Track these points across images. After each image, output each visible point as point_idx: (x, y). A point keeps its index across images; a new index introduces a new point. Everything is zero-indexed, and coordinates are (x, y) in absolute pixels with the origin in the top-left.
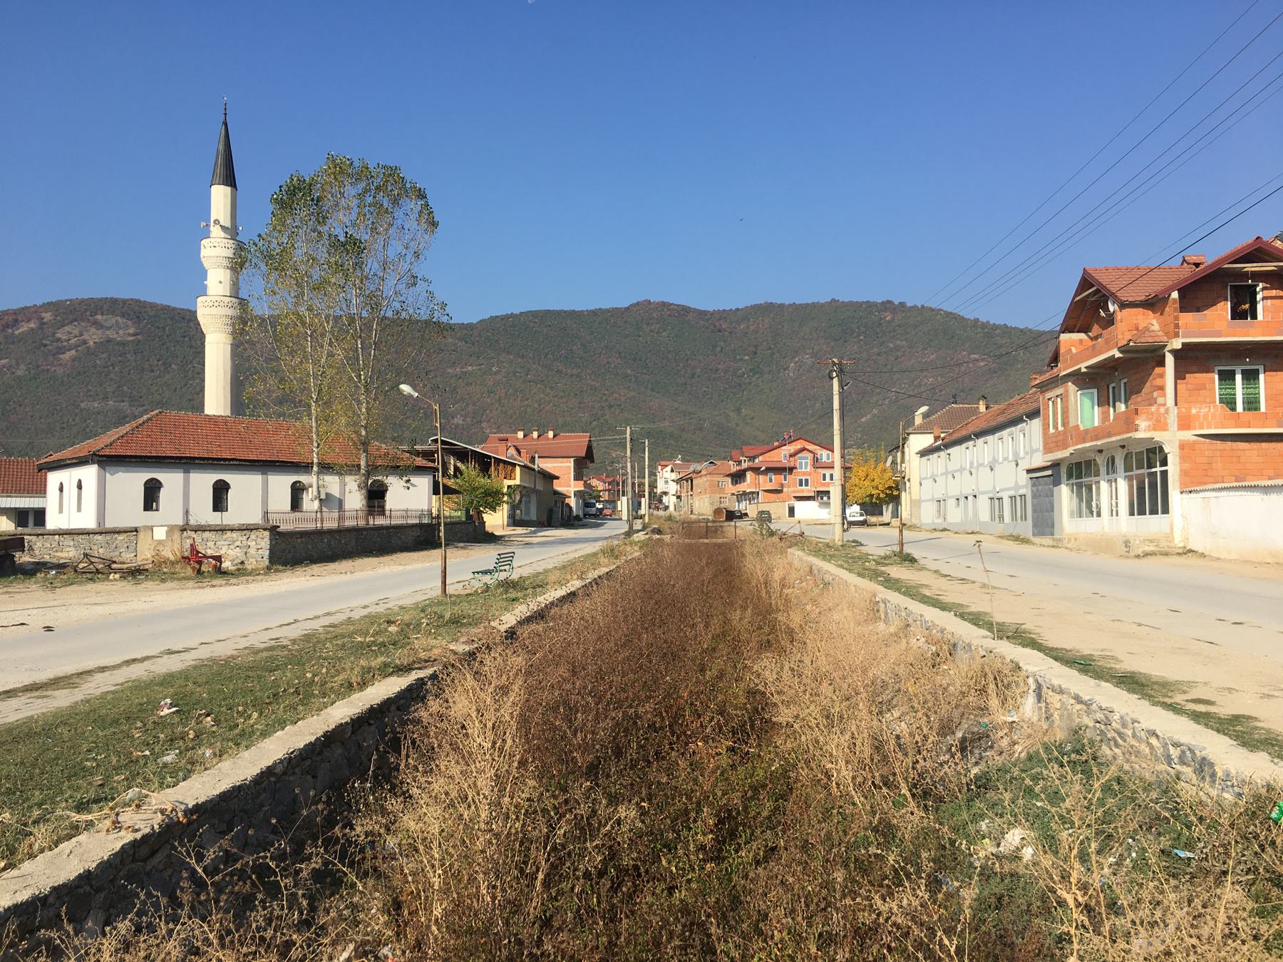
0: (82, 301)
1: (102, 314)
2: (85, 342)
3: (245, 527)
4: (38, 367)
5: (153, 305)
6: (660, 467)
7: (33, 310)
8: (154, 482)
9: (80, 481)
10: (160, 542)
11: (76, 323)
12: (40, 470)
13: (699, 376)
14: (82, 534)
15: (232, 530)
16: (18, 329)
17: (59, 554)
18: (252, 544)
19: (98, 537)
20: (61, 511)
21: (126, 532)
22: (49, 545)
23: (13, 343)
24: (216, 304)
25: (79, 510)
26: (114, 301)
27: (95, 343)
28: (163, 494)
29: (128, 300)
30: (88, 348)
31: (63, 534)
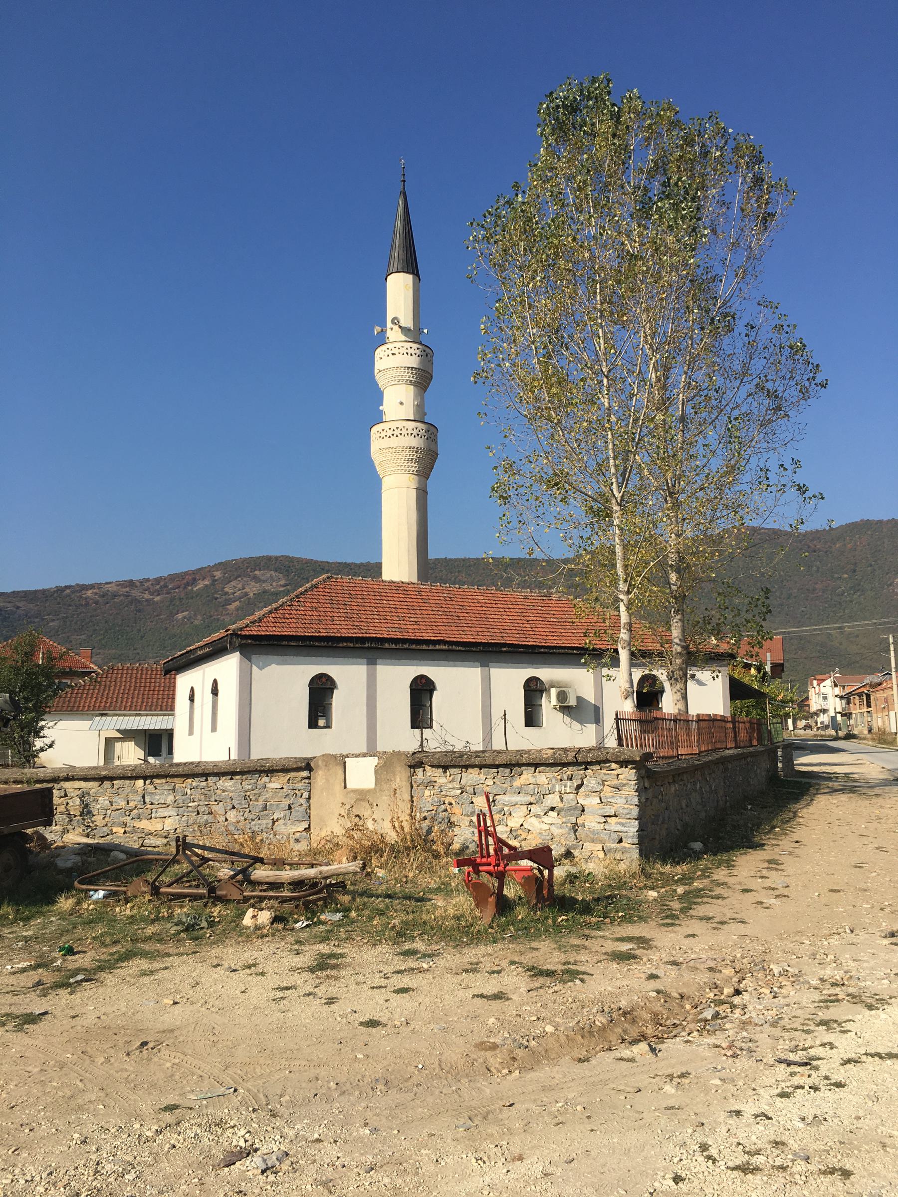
0: (245, 559)
1: (260, 570)
2: (246, 594)
3: (570, 757)
4: (211, 616)
5: (299, 560)
6: (815, 683)
7: (208, 569)
8: (324, 680)
9: (215, 682)
10: (362, 796)
11: (240, 579)
12: (167, 672)
13: (795, 597)
14: (193, 776)
15: (536, 765)
16: (196, 586)
17: (144, 824)
18: (591, 802)
19: (226, 783)
20: (191, 732)
21: (285, 770)
22: (123, 803)
23: (192, 598)
24: (397, 432)
25: (214, 729)
26: (269, 558)
27: (254, 594)
28: (338, 700)
29: (280, 557)
30: (249, 599)
31: (152, 777)
